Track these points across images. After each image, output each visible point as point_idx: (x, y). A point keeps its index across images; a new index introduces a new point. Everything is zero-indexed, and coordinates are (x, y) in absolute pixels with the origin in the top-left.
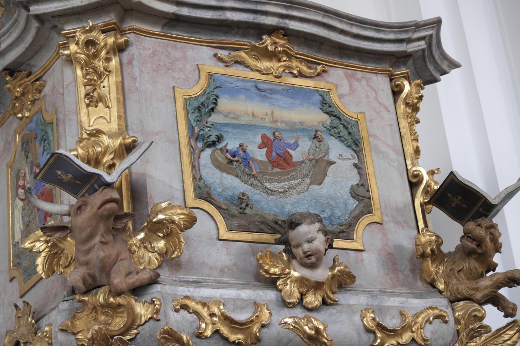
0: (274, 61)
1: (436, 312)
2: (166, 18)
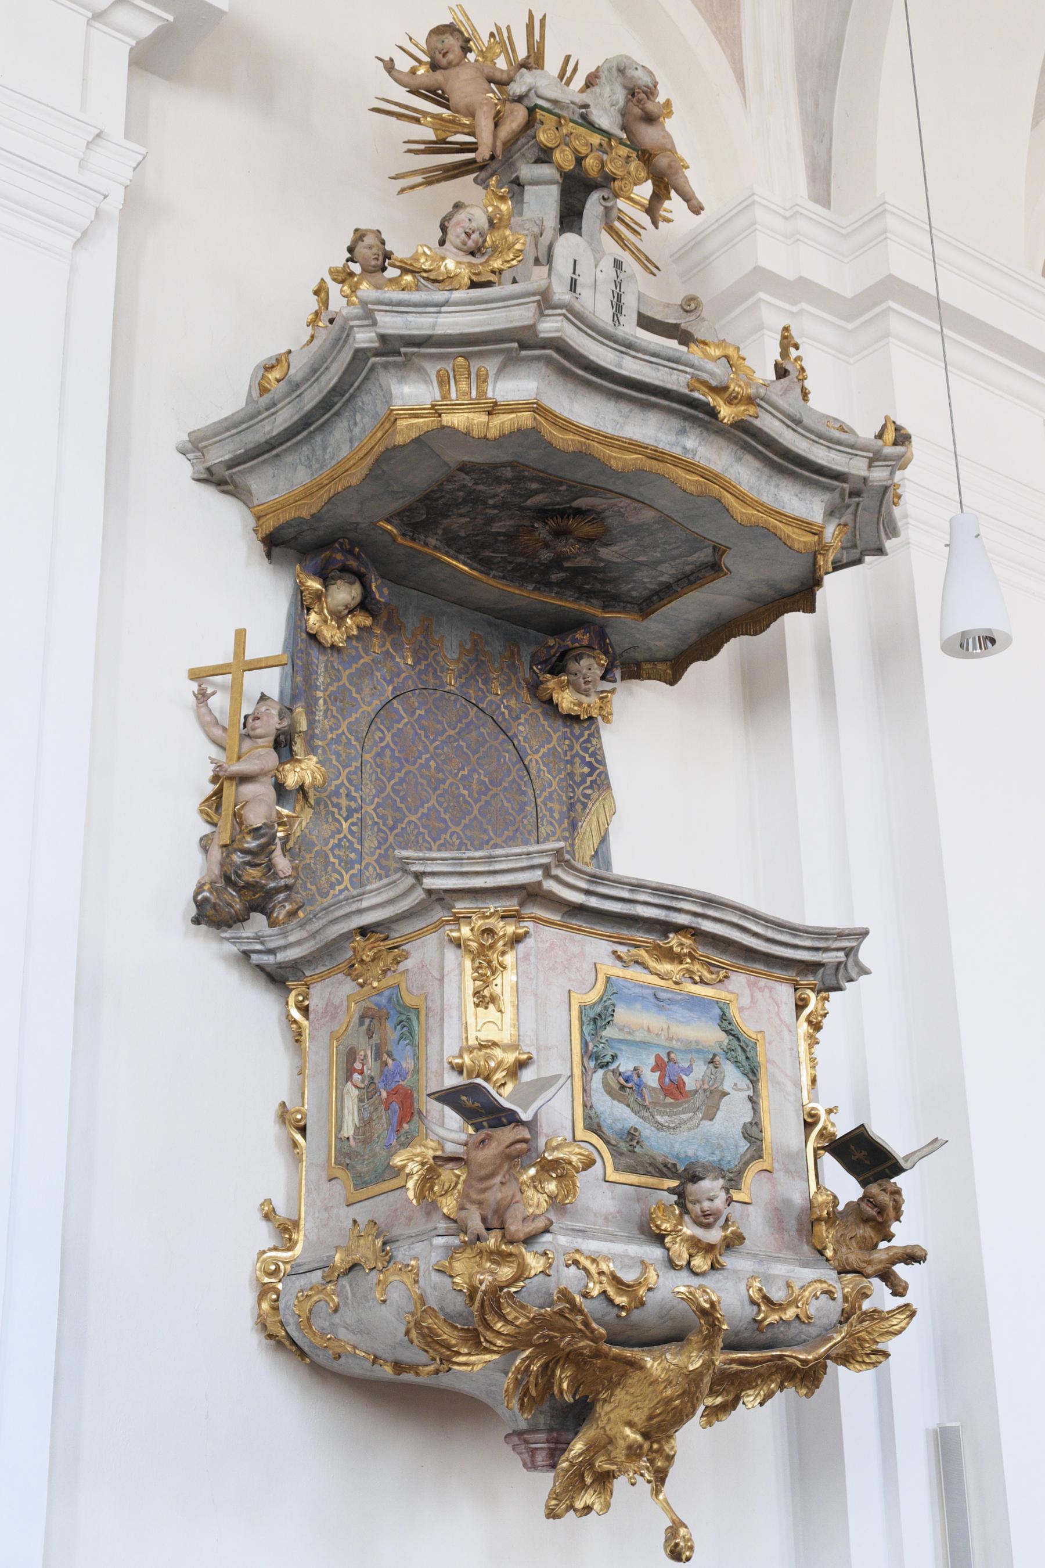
1: (825, 1286)
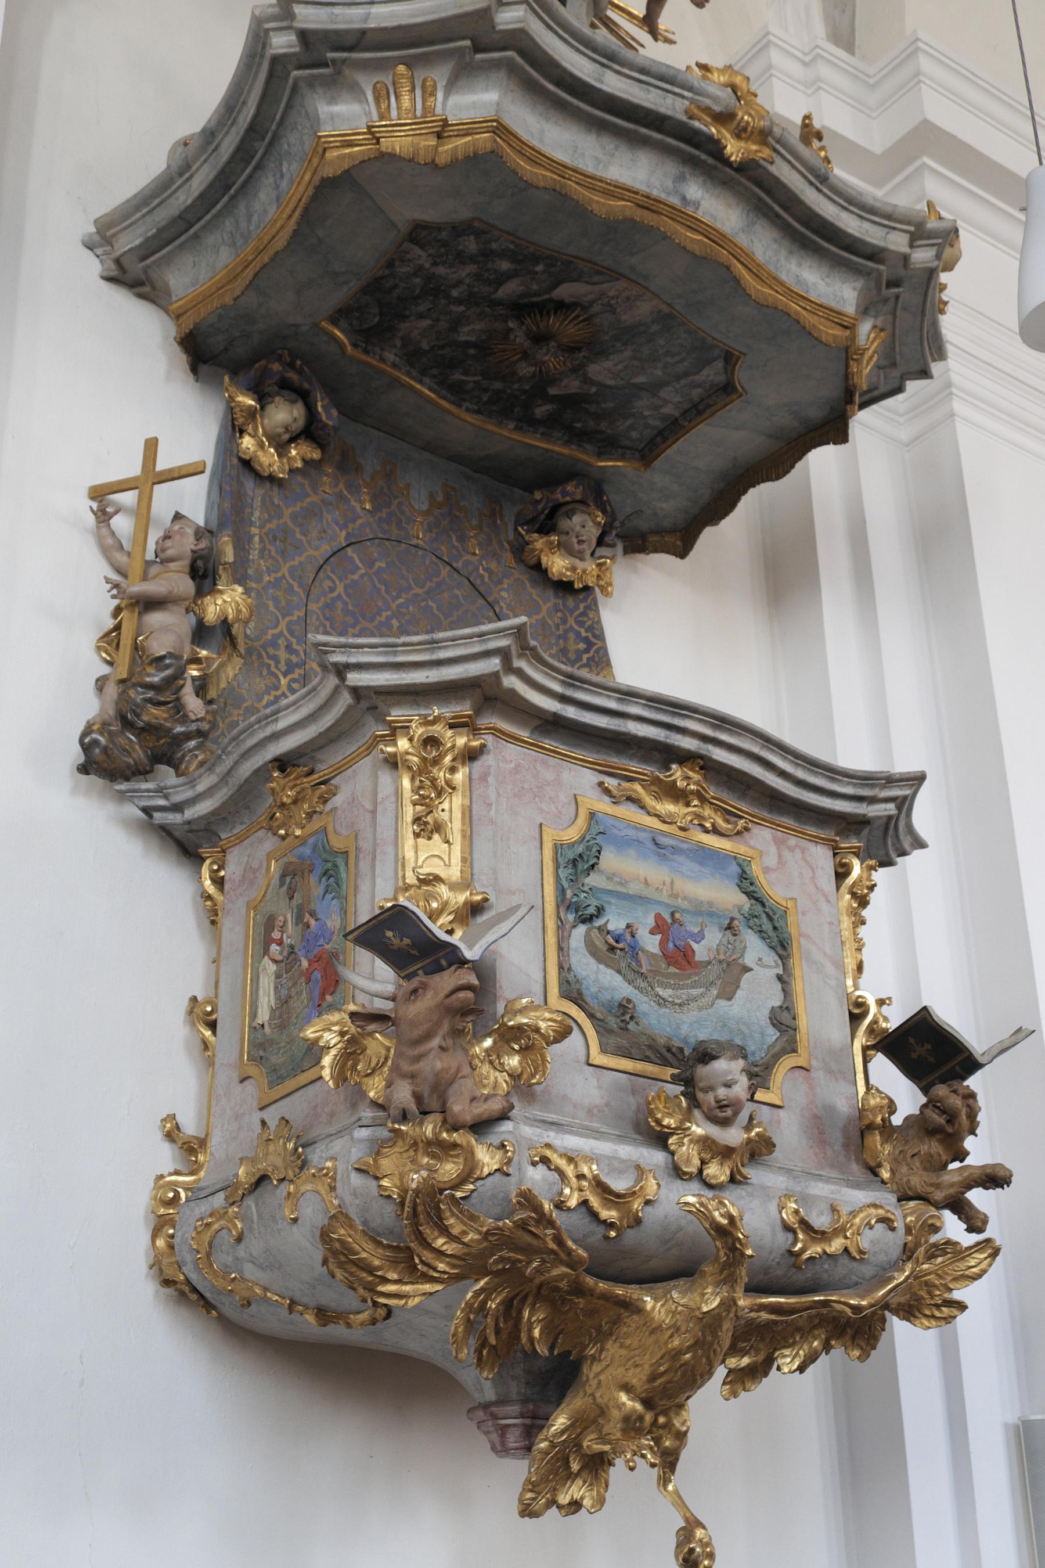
0: (680, 804)
1: (881, 1212)
2: (540, 718)
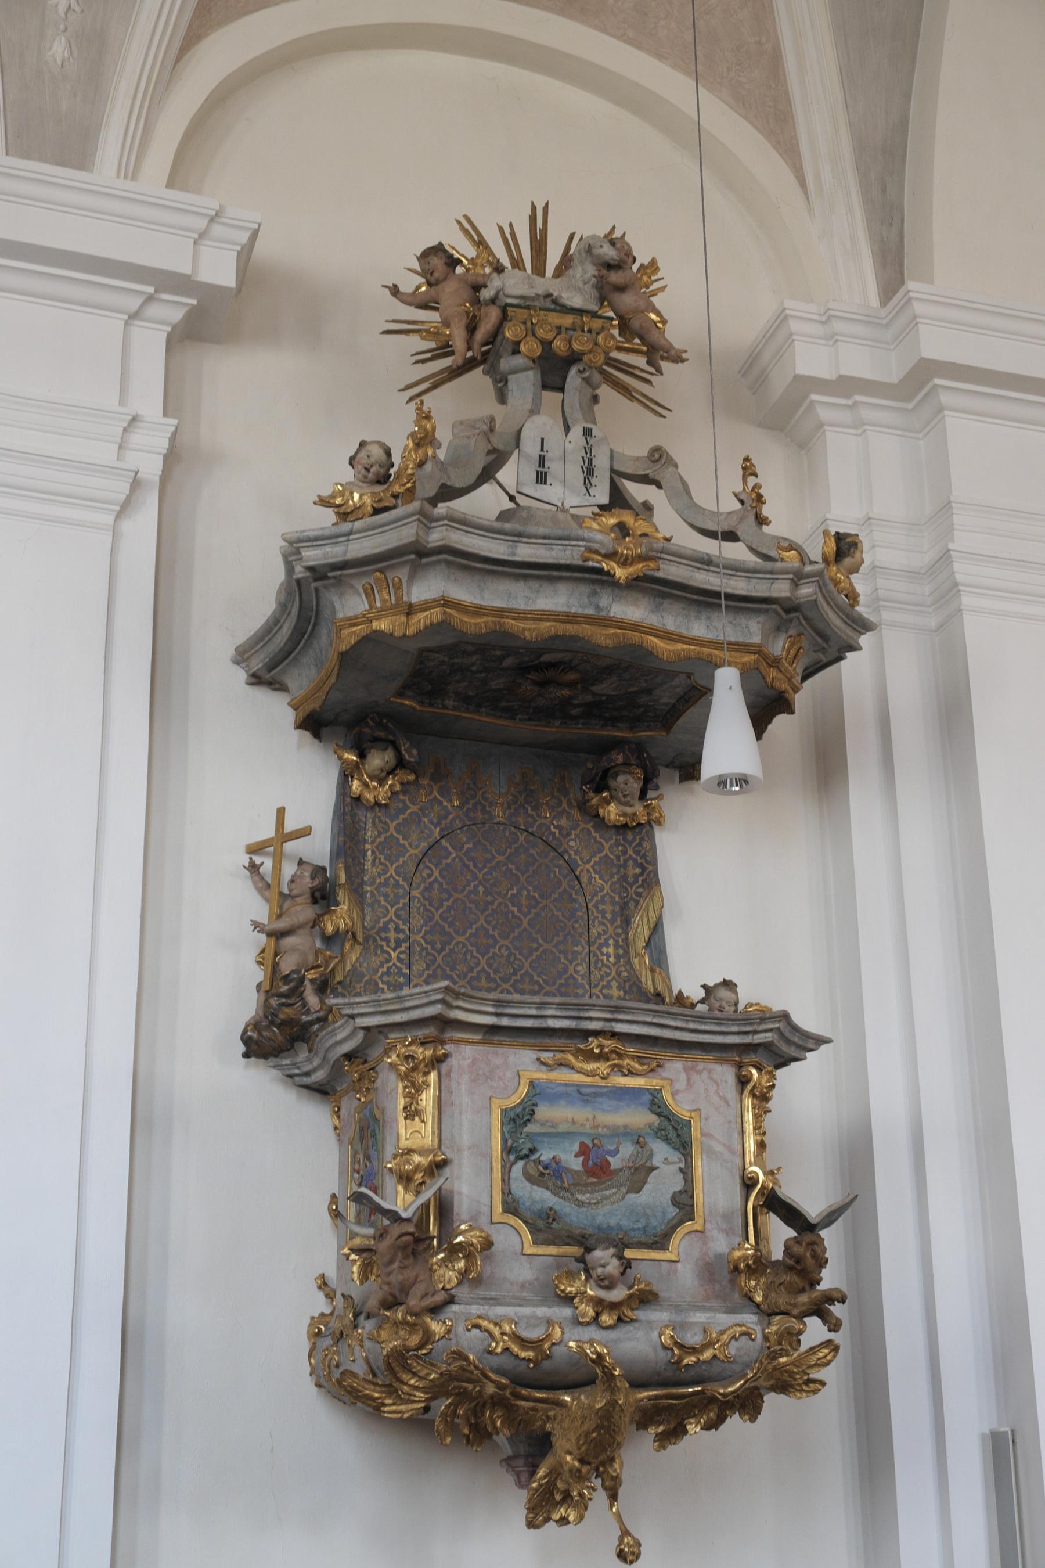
1: (744, 1328)
